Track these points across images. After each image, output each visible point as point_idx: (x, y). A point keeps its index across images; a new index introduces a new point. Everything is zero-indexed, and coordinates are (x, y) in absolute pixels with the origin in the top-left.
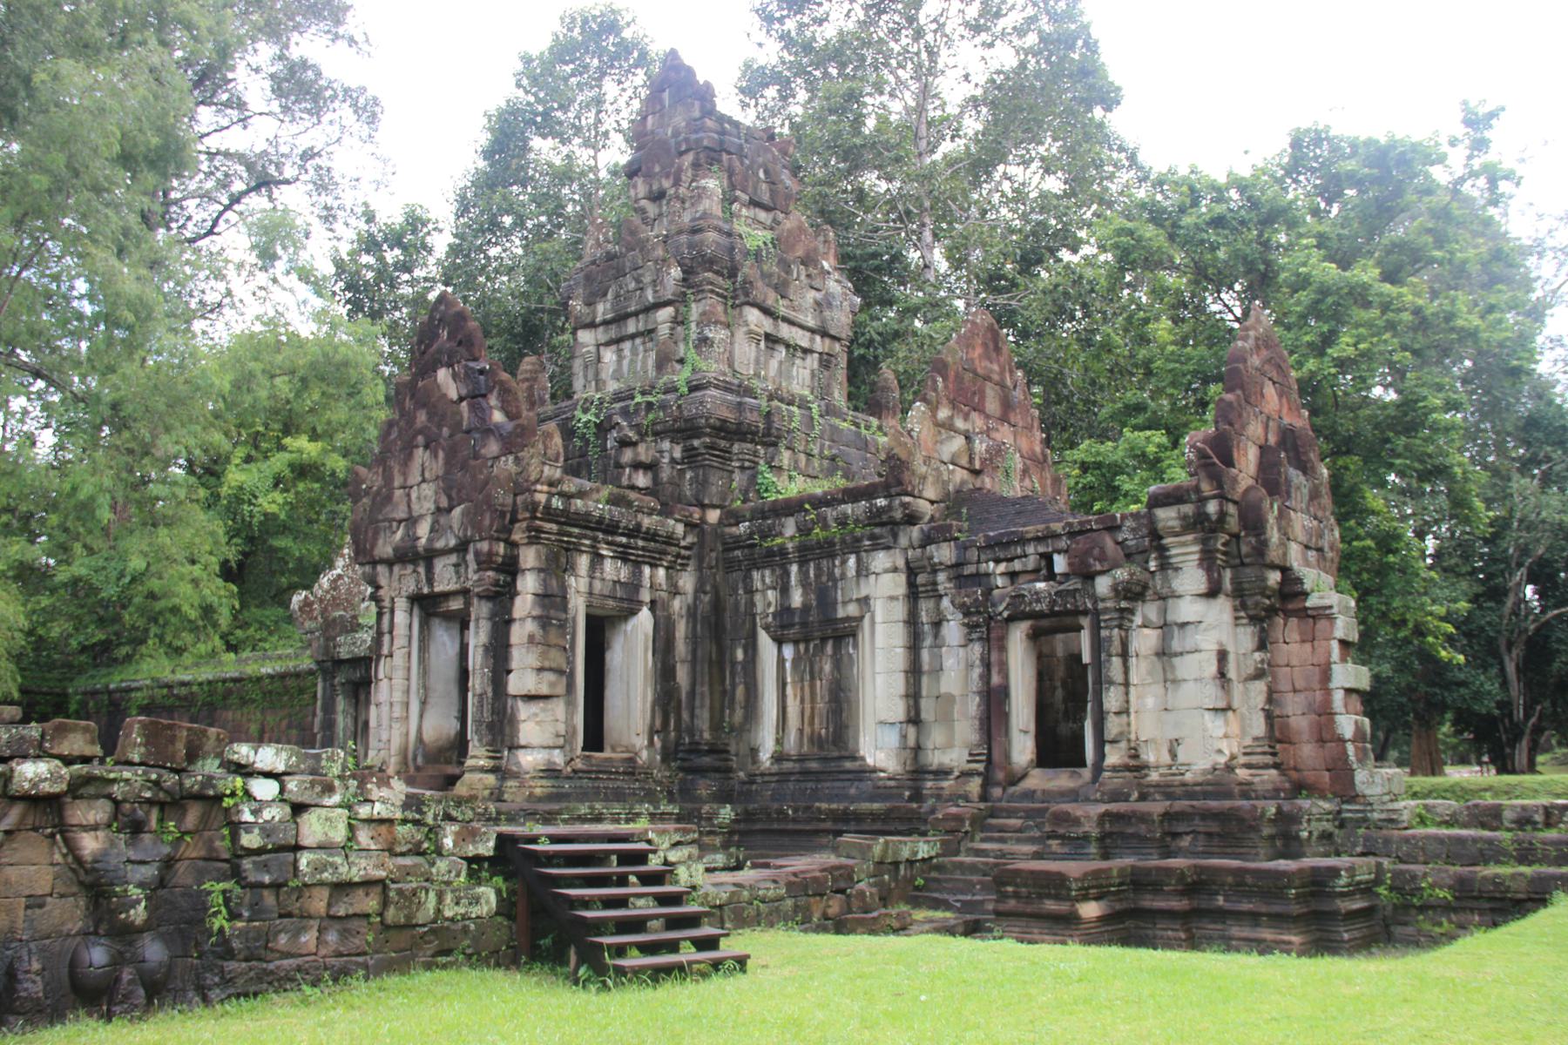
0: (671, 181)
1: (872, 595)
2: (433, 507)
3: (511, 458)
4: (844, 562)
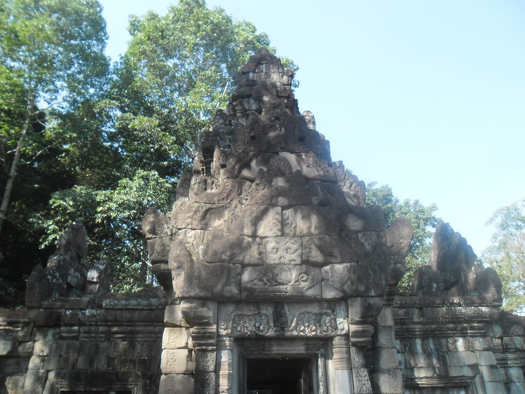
1: (479, 363)
2: (299, 261)
4: (455, 342)
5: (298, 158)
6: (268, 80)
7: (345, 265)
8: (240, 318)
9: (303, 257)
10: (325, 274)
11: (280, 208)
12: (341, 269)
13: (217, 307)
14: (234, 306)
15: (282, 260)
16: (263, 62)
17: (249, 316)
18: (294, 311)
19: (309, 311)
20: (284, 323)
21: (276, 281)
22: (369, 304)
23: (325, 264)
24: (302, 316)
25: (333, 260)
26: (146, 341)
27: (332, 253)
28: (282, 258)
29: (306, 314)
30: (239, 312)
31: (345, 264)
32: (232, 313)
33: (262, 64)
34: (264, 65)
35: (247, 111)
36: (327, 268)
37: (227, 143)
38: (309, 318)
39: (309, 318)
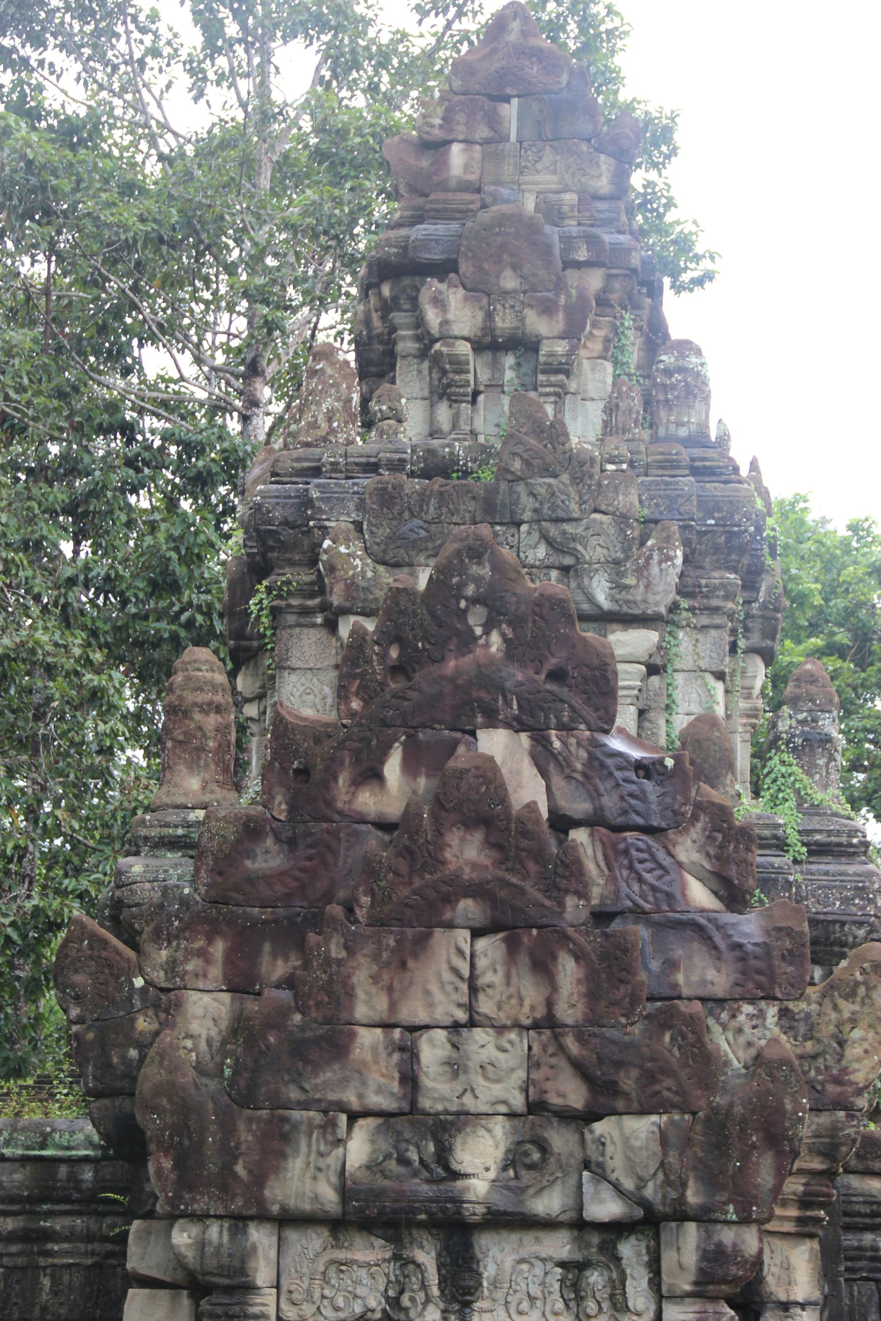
0: (558, 324)
2: (518, 1102)
3: (772, 1011)
5: (540, 748)
6: (530, 178)
7: (653, 1123)
8: (342, 1271)
9: (531, 1090)
10: (593, 1147)
11: (467, 934)
12: (643, 1135)
13: (275, 1239)
14: (327, 1233)
15: (468, 1101)
16: (509, 91)
17: (369, 1265)
18: (502, 1250)
19: (544, 1255)
20: (469, 1288)
21: (447, 1167)
22: (720, 1245)
23: (590, 1116)
24: (525, 1267)
25: (620, 1105)
26: (70, 1266)
27: (615, 1083)
28: (468, 1095)
29: (538, 1264)
30: (341, 1255)
31: (655, 1118)
32: (317, 1255)
33: (507, 99)
34: (515, 101)
35: (437, 340)
36: (600, 1127)
37: (348, 515)
38: (546, 1274)
39: (546, 1274)
